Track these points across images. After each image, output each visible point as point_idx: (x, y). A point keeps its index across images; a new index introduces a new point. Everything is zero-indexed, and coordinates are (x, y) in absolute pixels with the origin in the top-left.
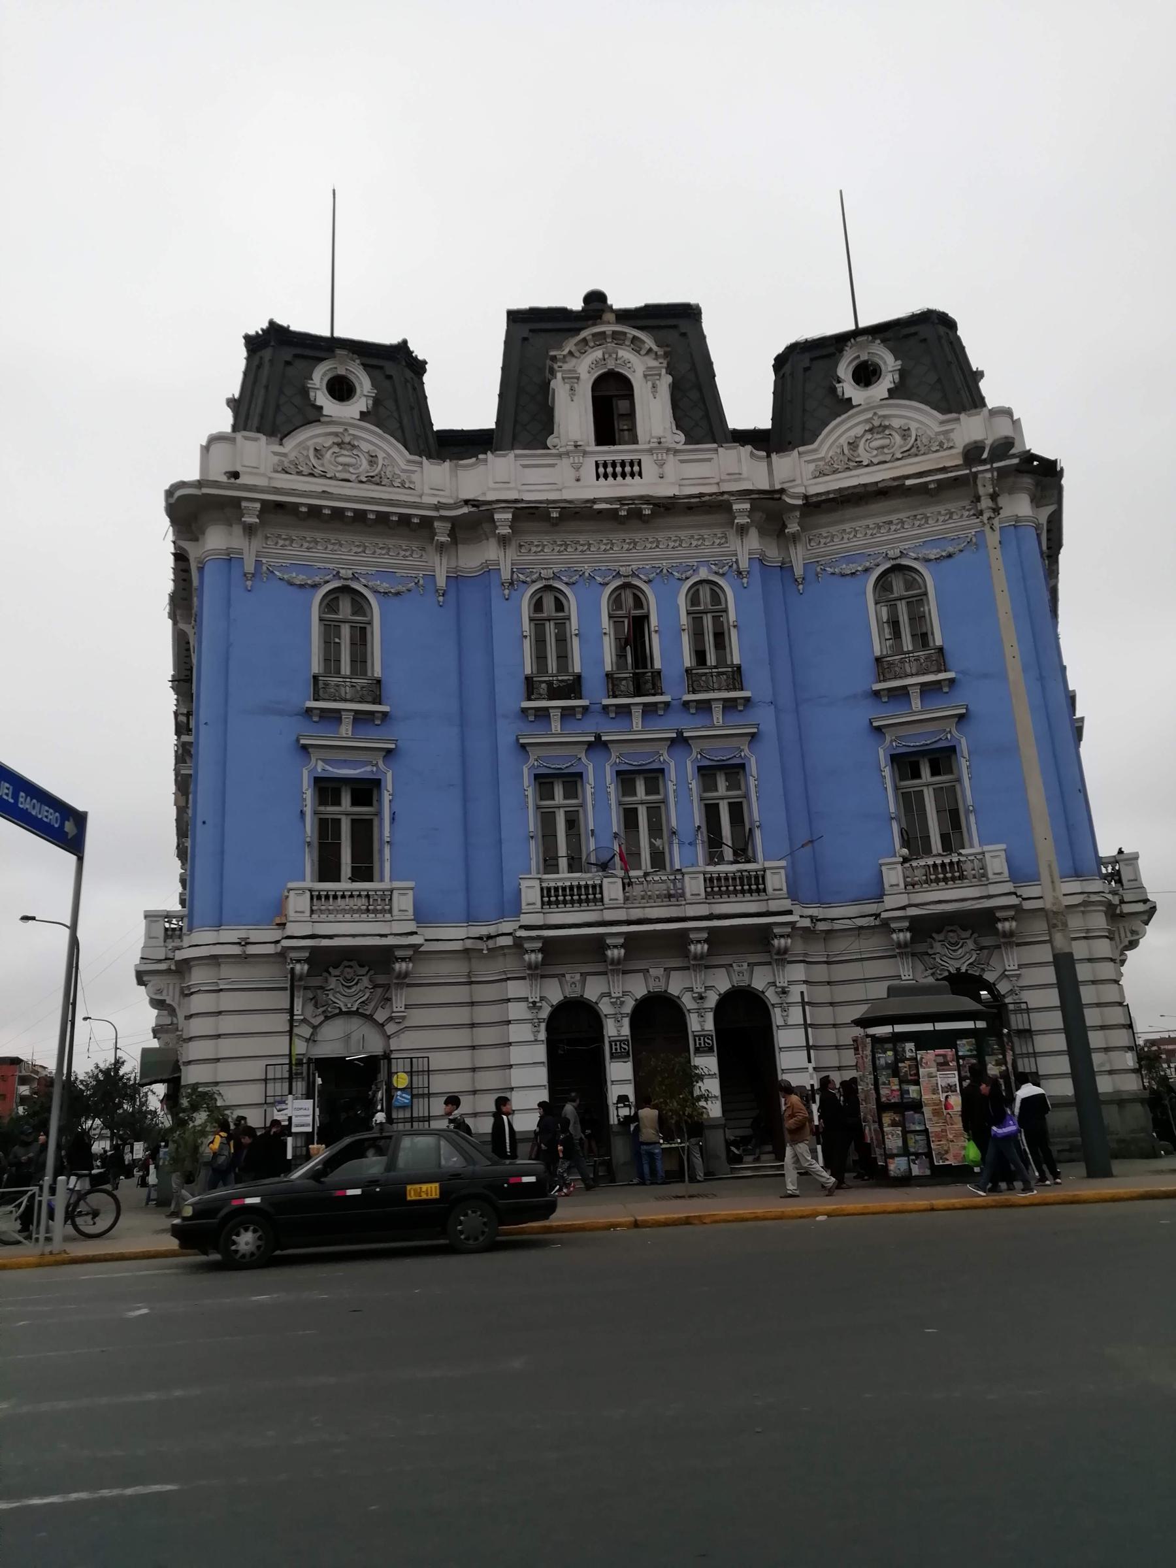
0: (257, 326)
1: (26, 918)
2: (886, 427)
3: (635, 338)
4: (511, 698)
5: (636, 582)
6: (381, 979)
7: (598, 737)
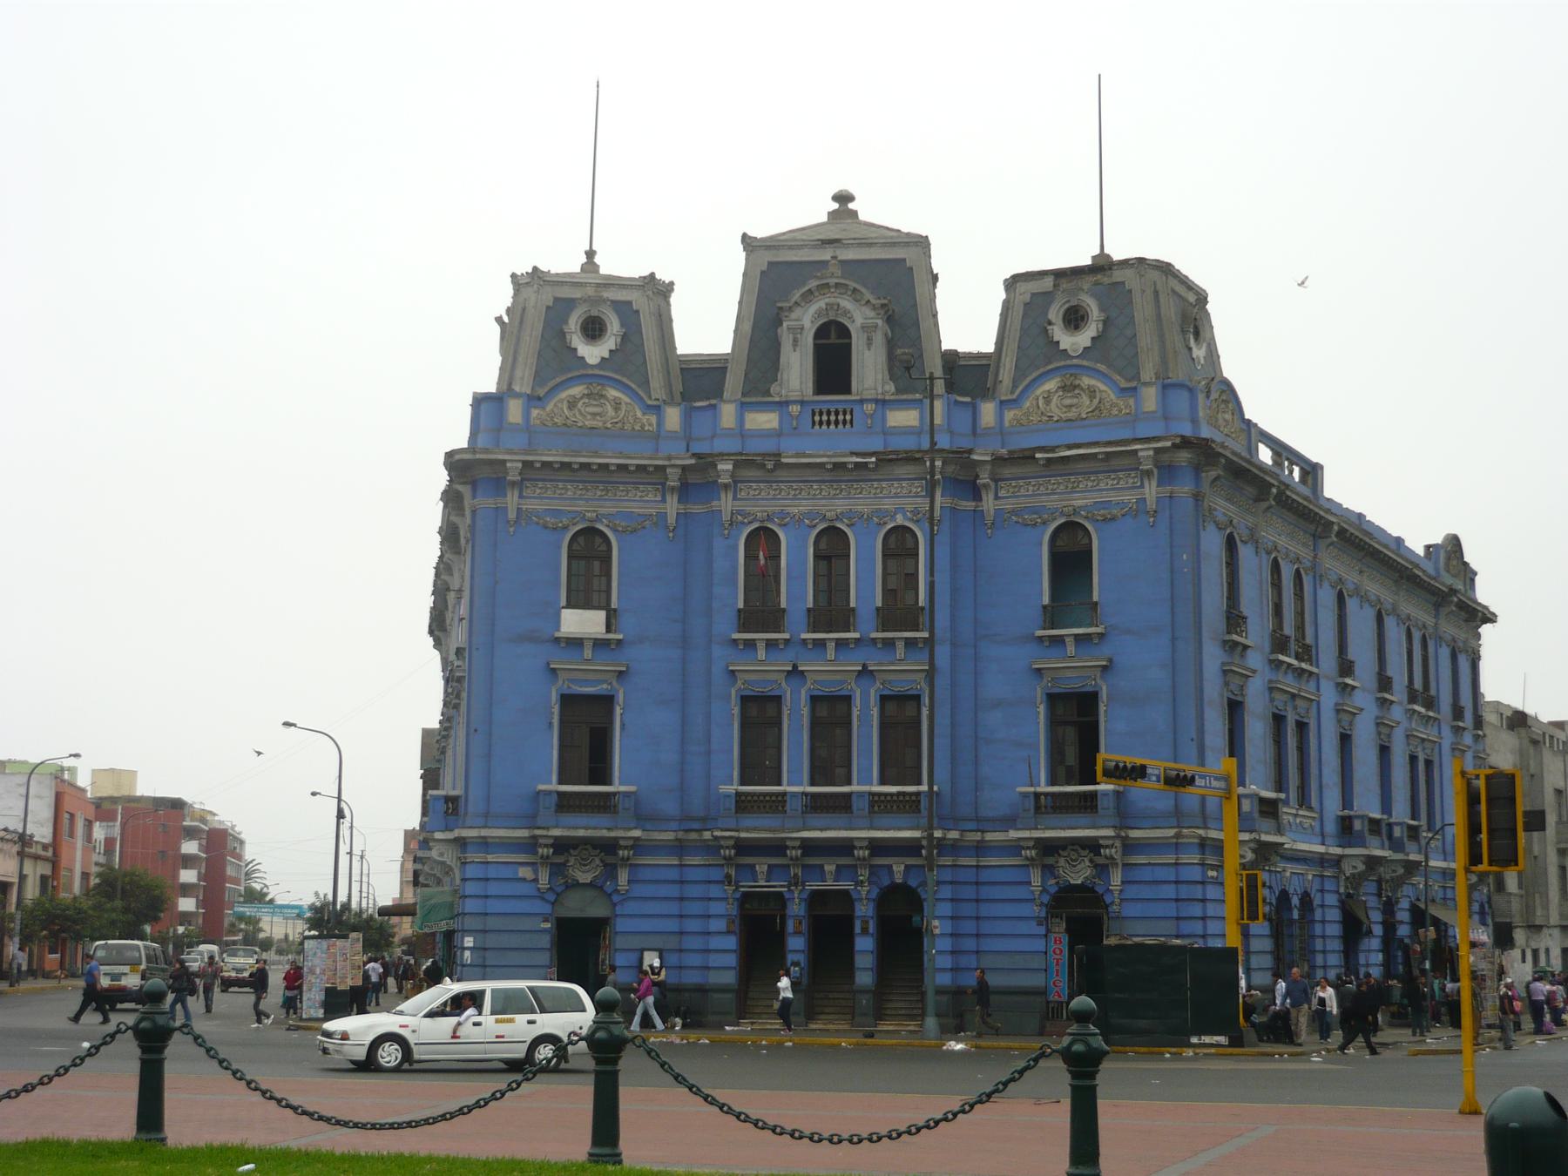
0: (524, 268)
1: (287, 724)
2: (1076, 387)
3: (855, 290)
4: (725, 625)
5: (839, 525)
6: (610, 860)
7: (795, 666)
